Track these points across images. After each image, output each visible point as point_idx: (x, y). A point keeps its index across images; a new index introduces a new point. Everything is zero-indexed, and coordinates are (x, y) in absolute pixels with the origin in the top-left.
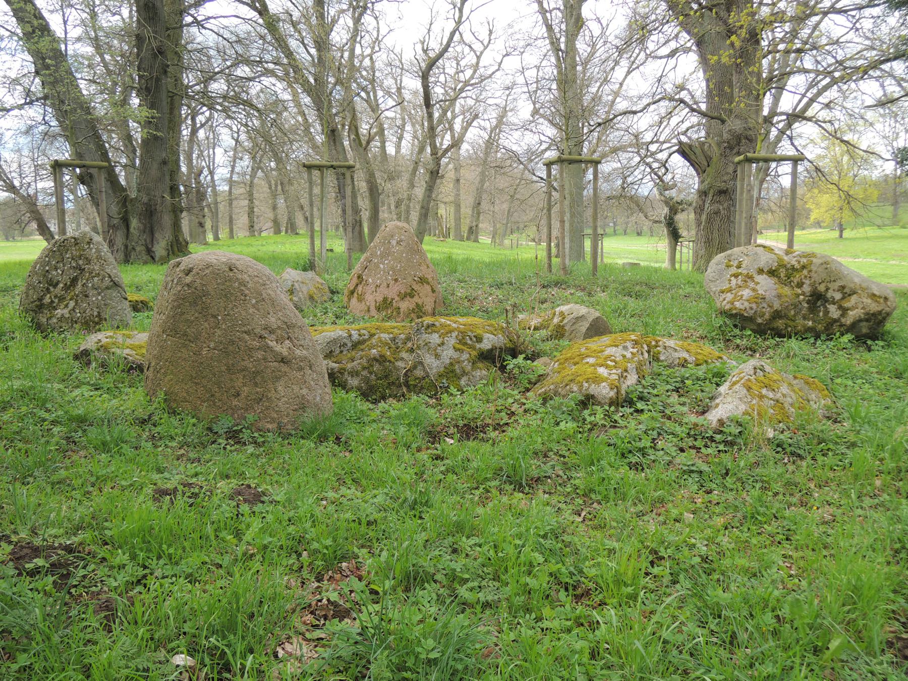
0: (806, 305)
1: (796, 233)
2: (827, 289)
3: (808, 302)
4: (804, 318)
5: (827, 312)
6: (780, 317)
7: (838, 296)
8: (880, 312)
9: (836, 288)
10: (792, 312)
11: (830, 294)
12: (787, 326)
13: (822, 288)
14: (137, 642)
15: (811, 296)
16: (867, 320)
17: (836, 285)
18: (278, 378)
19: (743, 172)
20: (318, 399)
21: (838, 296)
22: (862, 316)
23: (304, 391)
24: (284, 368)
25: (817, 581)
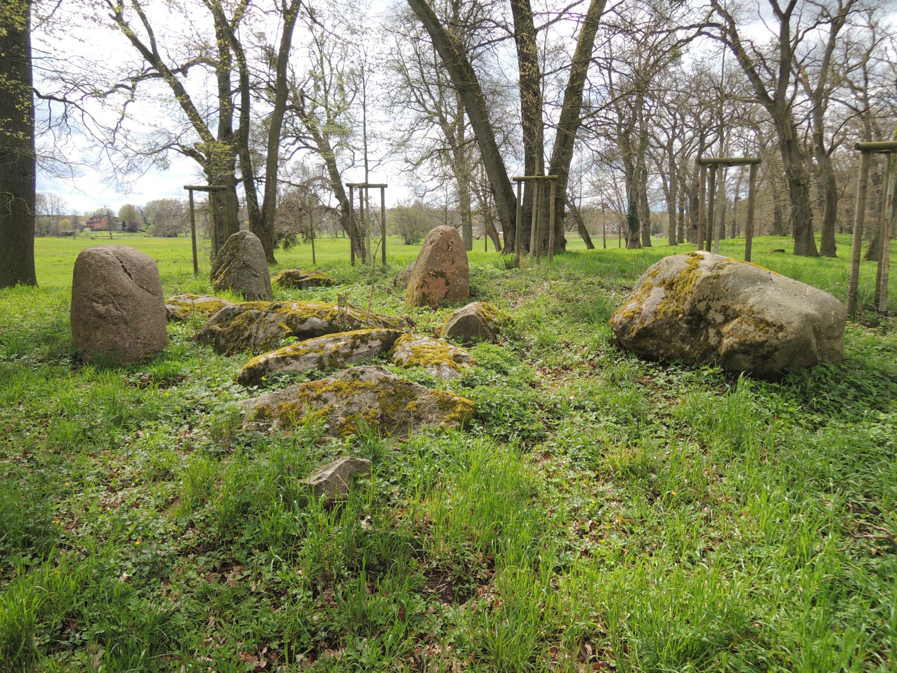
0: (685, 325)
1: (754, 240)
2: (708, 308)
3: (688, 322)
4: (683, 340)
5: (707, 338)
6: (653, 336)
7: (719, 318)
8: (761, 344)
9: (719, 308)
10: (668, 332)
11: (711, 315)
12: (659, 347)
13: (702, 307)
14: (849, 425)
15: (689, 315)
16: (746, 352)
17: (717, 305)
18: (97, 328)
19: (720, 176)
20: (127, 345)
21: (719, 318)
22: (736, 346)
23: (117, 339)
24: (101, 322)
25: (873, 550)
